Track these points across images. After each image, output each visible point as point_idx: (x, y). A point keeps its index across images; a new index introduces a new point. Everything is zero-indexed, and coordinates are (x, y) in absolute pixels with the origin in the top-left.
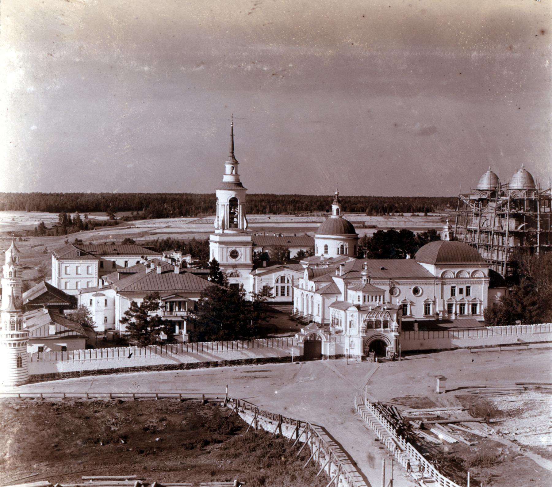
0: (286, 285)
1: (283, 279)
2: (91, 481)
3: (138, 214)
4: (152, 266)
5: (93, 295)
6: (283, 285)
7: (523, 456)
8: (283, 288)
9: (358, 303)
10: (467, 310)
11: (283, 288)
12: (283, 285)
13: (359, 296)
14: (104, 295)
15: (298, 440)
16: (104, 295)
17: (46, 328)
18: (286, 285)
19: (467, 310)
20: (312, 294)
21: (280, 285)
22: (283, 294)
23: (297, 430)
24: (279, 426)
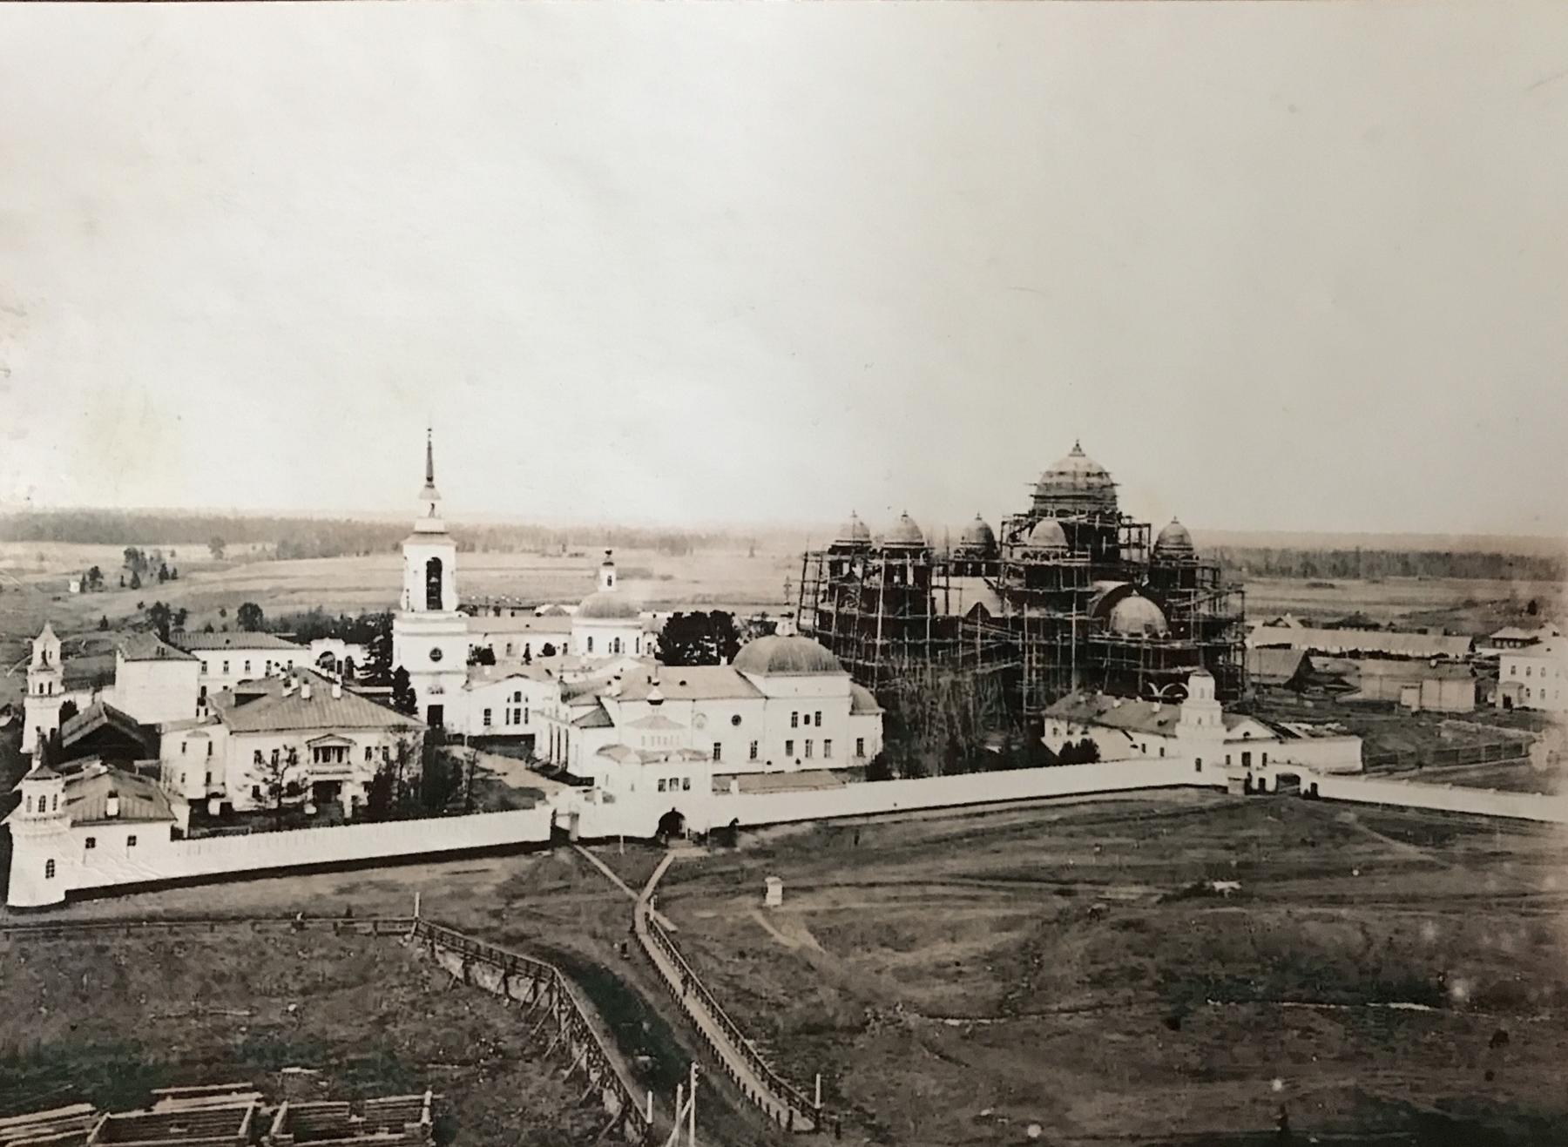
0: (522, 706)
1: (518, 696)
2: (169, 1099)
3: (264, 549)
4: (295, 683)
5: (188, 736)
6: (517, 705)
7: (1302, 618)
8: (517, 712)
9: (640, 748)
10: (818, 748)
11: (517, 712)
12: (517, 705)
13: (643, 738)
14: (207, 735)
15: (538, 1005)
16: (207, 735)
17: (102, 801)
18: (522, 706)
19: (818, 748)
20: (566, 727)
21: (513, 706)
22: (517, 721)
23: (535, 986)
24: (505, 980)
